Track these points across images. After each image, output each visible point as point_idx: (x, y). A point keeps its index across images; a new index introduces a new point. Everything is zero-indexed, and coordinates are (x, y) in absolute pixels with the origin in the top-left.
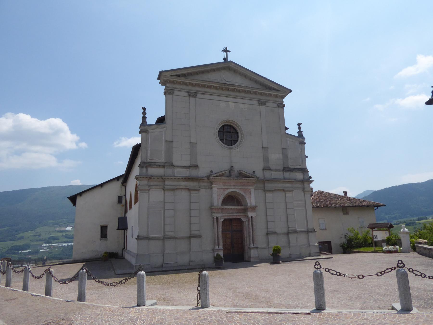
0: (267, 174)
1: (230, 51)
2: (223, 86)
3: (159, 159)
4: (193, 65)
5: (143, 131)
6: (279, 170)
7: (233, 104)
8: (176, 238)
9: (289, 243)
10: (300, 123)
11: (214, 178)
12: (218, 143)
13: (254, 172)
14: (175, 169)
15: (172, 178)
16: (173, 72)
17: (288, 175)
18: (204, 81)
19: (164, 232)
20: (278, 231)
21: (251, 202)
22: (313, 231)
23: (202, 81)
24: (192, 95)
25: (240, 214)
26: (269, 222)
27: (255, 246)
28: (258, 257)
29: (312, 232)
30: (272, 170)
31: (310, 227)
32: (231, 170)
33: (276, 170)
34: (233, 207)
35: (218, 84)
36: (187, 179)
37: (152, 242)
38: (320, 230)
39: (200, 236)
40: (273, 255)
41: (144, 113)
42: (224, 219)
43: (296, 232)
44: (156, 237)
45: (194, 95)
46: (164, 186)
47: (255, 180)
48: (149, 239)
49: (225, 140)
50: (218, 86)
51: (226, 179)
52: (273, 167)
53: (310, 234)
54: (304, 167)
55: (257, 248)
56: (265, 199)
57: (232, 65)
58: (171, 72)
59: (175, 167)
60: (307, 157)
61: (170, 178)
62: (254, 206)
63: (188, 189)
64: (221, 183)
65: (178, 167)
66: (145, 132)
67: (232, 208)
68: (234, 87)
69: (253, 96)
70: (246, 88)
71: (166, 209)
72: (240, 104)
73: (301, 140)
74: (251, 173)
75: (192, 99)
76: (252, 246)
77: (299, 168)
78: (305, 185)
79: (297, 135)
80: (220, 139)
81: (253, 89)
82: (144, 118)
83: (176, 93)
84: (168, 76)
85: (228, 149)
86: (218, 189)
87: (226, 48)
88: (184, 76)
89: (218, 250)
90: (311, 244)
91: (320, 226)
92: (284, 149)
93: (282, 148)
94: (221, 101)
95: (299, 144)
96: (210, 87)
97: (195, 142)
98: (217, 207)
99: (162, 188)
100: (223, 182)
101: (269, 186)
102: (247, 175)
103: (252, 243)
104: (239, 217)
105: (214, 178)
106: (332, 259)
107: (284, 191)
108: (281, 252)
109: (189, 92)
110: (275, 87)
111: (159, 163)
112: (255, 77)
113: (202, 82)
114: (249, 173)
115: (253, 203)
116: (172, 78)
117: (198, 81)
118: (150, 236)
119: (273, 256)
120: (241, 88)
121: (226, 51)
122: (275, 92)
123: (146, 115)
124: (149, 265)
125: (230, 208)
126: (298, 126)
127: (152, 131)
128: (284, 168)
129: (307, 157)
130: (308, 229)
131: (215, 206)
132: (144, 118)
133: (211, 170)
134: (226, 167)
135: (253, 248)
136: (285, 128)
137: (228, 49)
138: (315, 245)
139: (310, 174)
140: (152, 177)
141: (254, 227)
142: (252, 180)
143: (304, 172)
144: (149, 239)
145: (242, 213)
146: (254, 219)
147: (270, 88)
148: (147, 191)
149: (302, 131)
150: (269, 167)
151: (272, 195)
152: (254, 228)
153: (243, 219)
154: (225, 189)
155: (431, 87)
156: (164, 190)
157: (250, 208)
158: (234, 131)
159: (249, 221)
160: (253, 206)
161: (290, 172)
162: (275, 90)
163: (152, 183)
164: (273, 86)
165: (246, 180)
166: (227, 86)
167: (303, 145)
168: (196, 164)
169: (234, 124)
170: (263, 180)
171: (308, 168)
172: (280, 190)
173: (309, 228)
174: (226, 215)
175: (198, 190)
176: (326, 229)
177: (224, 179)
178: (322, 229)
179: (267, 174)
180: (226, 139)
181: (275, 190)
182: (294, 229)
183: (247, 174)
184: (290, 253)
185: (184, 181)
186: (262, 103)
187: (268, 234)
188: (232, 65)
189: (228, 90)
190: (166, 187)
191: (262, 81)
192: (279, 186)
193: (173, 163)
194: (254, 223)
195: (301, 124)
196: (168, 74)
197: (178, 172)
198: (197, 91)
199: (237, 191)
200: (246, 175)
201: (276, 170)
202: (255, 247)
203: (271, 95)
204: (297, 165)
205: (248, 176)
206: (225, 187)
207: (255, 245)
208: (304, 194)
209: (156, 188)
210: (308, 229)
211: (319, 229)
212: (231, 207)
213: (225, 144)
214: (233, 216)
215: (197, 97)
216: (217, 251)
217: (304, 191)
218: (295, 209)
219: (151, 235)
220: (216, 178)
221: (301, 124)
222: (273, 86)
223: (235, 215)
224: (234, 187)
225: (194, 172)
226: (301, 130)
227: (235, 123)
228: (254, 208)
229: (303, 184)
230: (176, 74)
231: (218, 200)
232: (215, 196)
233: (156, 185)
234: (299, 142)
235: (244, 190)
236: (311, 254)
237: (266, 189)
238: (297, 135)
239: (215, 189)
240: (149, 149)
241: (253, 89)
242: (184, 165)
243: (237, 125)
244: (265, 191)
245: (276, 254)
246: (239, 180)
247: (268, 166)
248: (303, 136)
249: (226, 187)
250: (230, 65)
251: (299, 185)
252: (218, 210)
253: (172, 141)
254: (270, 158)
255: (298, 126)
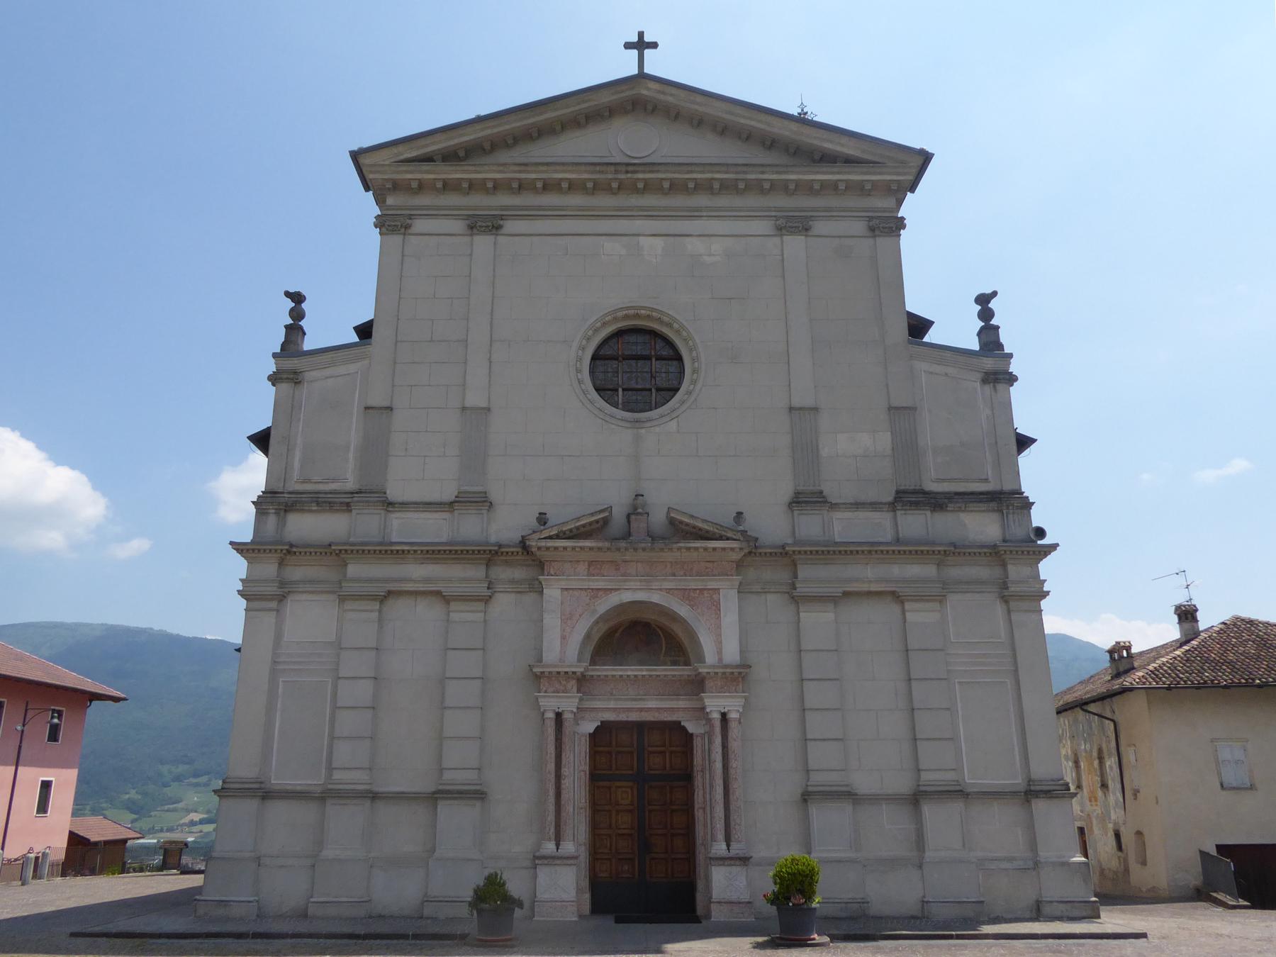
0: (811, 525)
1: (654, 45)
2: (610, 176)
3: (334, 480)
4: (483, 113)
5: (281, 379)
6: (874, 506)
7: (659, 242)
8: (374, 797)
9: (920, 842)
10: (989, 291)
11: (543, 543)
12: (583, 404)
13: (740, 514)
14: (393, 515)
15: (369, 551)
16: (401, 148)
17: (915, 523)
18: (526, 165)
19: (330, 769)
20: (864, 783)
21: (721, 649)
22: (1058, 791)
23: (517, 168)
24: (487, 225)
25: (675, 702)
26: (815, 740)
27: (736, 849)
28: (749, 903)
29: (1048, 794)
30: (834, 506)
31: (1041, 771)
32: (637, 509)
33: (858, 505)
34: (642, 671)
35: (586, 172)
36: (433, 553)
37: (279, 811)
38: (1224, 793)
39: (478, 795)
40: (775, 900)
41: (297, 314)
42: (602, 722)
43: (961, 791)
44: (299, 788)
45: (487, 227)
46: (340, 582)
47: (741, 549)
48: (266, 794)
49: (623, 390)
50: (590, 180)
51: (600, 549)
52: (832, 491)
53: (1040, 806)
54: (1007, 487)
55: (744, 860)
56: (798, 636)
57: (648, 89)
58: (395, 150)
59: (389, 505)
60: (1024, 442)
61: (363, 551)
62: (737, 666)
63: (438, 593)
64: (582, 568)
65: (405, 506)
66: (287, 378)
67: (636, 676)
68: (658, 171)
69: (752, 201)
70: (712, 172)
71: (805, 676)
72: (688, 239)
73: (989, 363)
74: (729, 521)
75: (483, 242)
76: (720, 848)
77: (982, 493)
78: (1010, 567)
79: (975, 346)
80: (597, 390)
81: (745, 173)
82: (294, 331)
83: (510, 226)
84: (383, 165)
85: (628, 425)
86: (566, 593)
87: (641, 35)
88: (450, 156)
89: (553, 858)
90: (1044, 854)
91: (1219, 774)
92: (897, 408)
93: (890, 408)
94: (604, 238)
95: (978, 385)
96: (548, 187)
97: (484, 405)
98: (557, 670)
99: (788, 593)
100: (591, 563)
101: (812, 575)
102: (700, 529)
103: (720, 835)
104: (674, 718)
105: (543, 543)
106: (1142, 941)
107: (896, 597)
108: (819, 888)
109: (871, 218)
110: (849, 149)
111: (331, 493)
112: (753, 123)
113: (520, 172)
114: (705, 521)
115: (731, 653)
116: (398, 172)
117: (501, 168)
118: (272, 782)
119: (778, 909)
120: (692, 172)
121: (641, 45)
122: (849, 173)
123: (993, 320)
124: (249, 902)
125: (629, 673)
126: (979, 307)
127: (314, 374)
128: (898, 492)
129: (1024, 442)
130: (1030, 781)
131: (548, 666)
132: (294, 331)
133: (540, 514)
134: (616, 498)
135: (722, 860)
136: (906, 316)
137: (647, 39)
138: (1066, 865)
139: (1038, 518)
140: (294, 550)
141: (733, 764)
142: (724, 549)
143: (1008, 508)
144: (266, 794)
145: (683, 700)
146: (734, 730)
147: (827, 159)
148: (274, 604)
149: (998, 327)
150: (821, 492)
151: (831, 616)
152: (734, 766)
153: (691, 727)
154: (601, 593)
155: (640, 30)
156: (343, 599)
157: (716, 673)
158: (666, 352)
159: (710, 734)
160: (726, 666)
161: (928, 513)
162: (849, 161)
163: (296, 573)
164: (839, 148)
165: (696, 549)
166: (627, 172)
167: (1000, 387)
168: (481, 492)
169: (659, 320)
170: (780, 551)
171: (1028, 488)
172: (879, 594)
173: (1033, 776)
174: (612, 705)
175: (487, 600)
176: (1252, 787)
177: (591, 549)
178: (1235, 784)
179: (811, 525)
180: (624, 387)
181: (847, 594)
182: (950, 776)
183: (700, 525)
184: (924, 897)
185: (422, 563)
186: (795, 225)
187: (806, 797)
188: (648, 89)
189: (633, 189)
190: (802, 589)
191: (787, 133)
192: (868, 574)
193: (385, 493)
194: (734, 745)
195: (994, 294)
196: (384, 157)
197: (402, 527)
198: (502, 210)
199: (655, 598)
200: (694, 527)
201: (858, 505)
202: (733, 853)
203: (833, 187)
204: (967, 481)
205: (707, 532)
206: (597, 580)
207: (734, 846)
208: (1009, 612)
209: (312, 592)
210: (1030, 781)
211: (1219, 786)
212: (632, 670)
213: (620, 406)
214: (641, 710)
215: (815, 231)
216: (546, 862)
217: (1005, 600)
218: (959, 683)
219: (277, 781)
220: (551, 543)
221: (994, 294)
222: (842, 145)
223: (652, 704)
224: (641, 581)
225: (470, 527)
226: (994, 322)
227: (666, 319)
228: (737, 677)
229: (1004, 565)
230: (414, 154)
231: (563, 638)
232: (552, 622)
233: (311, 582)
234: (979, 376)
235: (687, 595)
236: (1047, 910)
237: (802, 589)
238: (975, 346)
239: (553, 593)
240: (299, 441)
241: (745, 169)
242: (427, 499)
243: (675, 325)
244: (796, 600)
245: (789, 899)
246: (662, 550)
247: (819, 488)
248: (1000, 346)
249: (601, 585)
250: (645, 92)
251: (981, 571)
252: (565, 682)
253: (390, 409)
254: (825, 452)
255: (979, 307)
